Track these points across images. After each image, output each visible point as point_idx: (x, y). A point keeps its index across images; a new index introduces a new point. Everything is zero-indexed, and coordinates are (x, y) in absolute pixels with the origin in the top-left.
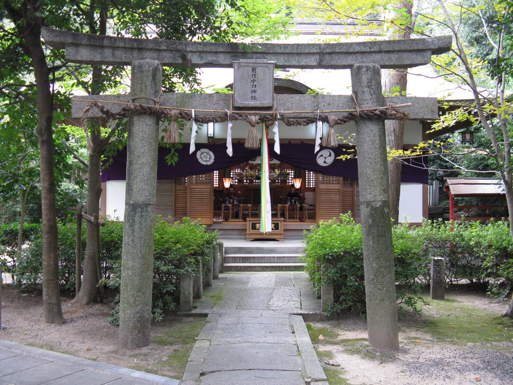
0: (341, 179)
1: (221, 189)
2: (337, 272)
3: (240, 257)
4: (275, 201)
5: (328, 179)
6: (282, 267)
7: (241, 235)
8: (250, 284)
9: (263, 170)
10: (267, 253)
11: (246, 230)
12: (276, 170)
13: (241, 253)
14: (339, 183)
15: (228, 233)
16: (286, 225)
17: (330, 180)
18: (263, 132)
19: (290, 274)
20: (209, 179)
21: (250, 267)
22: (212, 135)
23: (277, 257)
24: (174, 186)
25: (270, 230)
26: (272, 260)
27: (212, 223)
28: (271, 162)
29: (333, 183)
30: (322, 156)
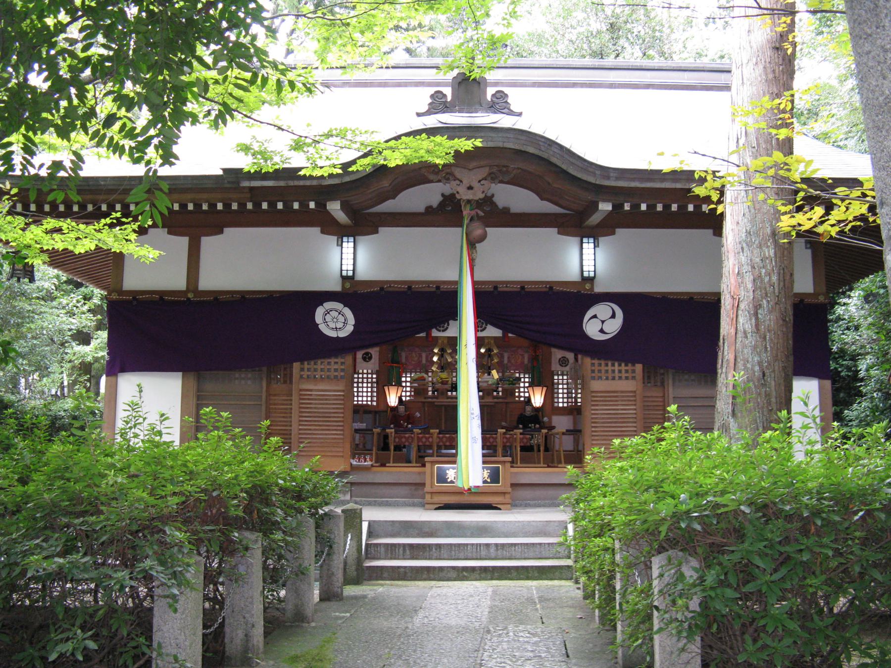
0: (639, 367)
1: (382, 408)
2: (722, 583)
3: (404, 545)
4: (488, 429)
5: (610, 368)
6: (509, 569)
7: (413, 496)
8: (421, 614)
9: (463, 343)
10: (472, 536)
11: (423, 485)
12: (494, 372)
13: (408, 536)
14: (634, 378)
15: (378, 493)
16: (516, 473)
17: (613, 371)
18: (461, 257)
19: (528, 588)
20: (342, 370)
21: (428, 569)
22: (350, 273)
23: (496, 545)
24: (264, 384)
25: (479, 483)
26: (483, 553)
27: (348, 469)
28: (480, 334)
29: (620, 378)
30: (595, 316)
